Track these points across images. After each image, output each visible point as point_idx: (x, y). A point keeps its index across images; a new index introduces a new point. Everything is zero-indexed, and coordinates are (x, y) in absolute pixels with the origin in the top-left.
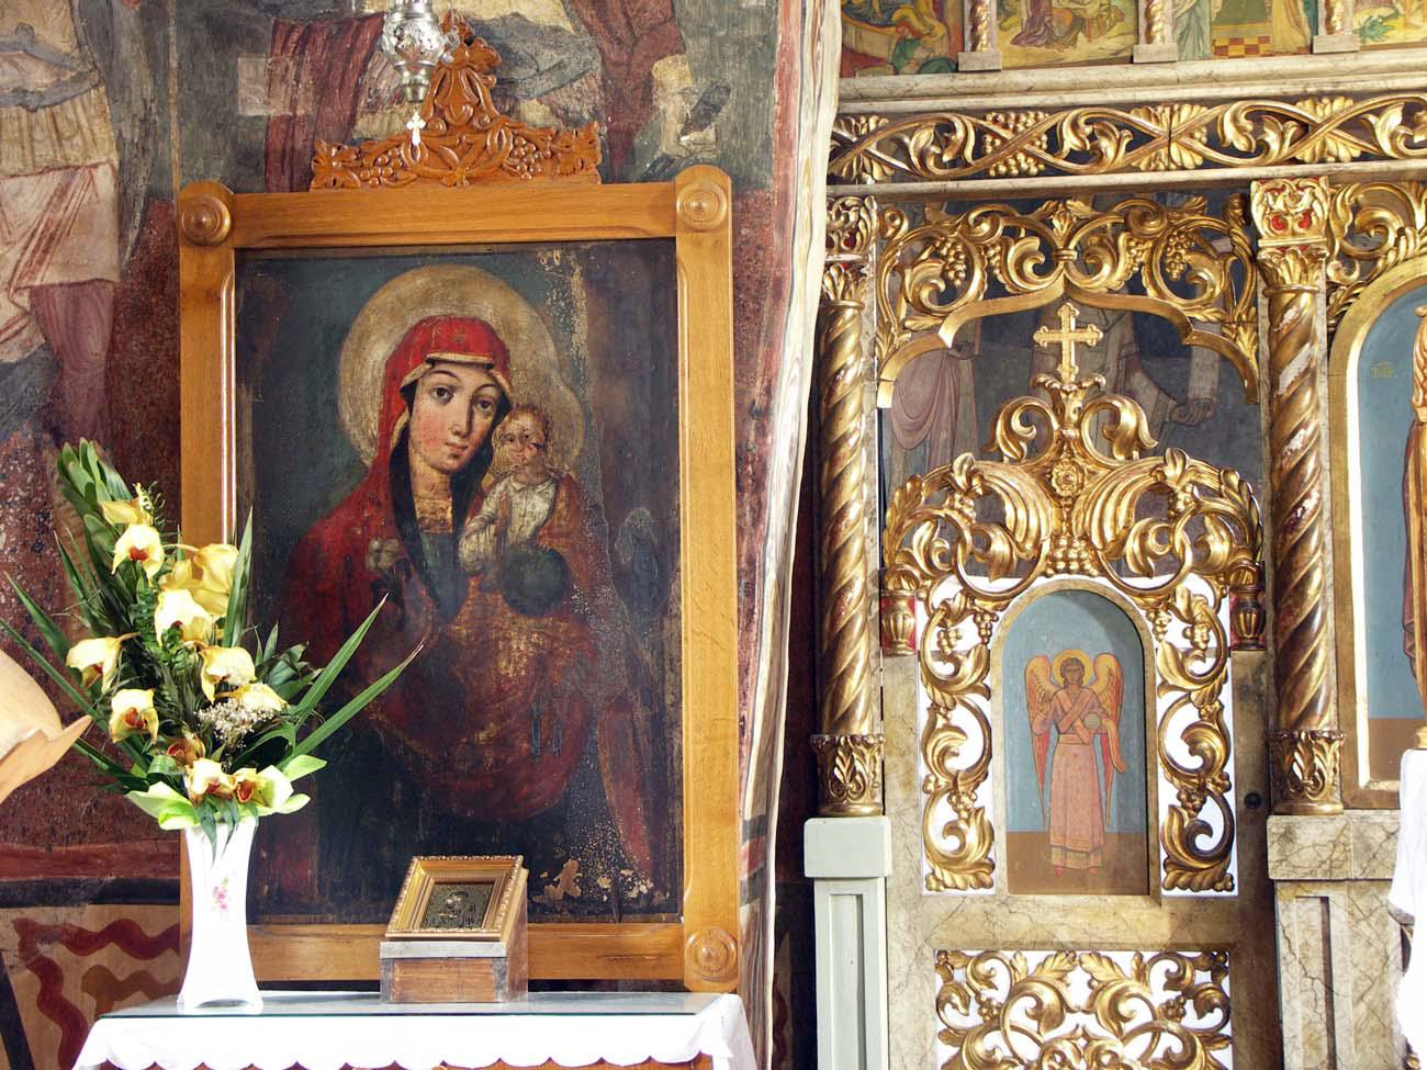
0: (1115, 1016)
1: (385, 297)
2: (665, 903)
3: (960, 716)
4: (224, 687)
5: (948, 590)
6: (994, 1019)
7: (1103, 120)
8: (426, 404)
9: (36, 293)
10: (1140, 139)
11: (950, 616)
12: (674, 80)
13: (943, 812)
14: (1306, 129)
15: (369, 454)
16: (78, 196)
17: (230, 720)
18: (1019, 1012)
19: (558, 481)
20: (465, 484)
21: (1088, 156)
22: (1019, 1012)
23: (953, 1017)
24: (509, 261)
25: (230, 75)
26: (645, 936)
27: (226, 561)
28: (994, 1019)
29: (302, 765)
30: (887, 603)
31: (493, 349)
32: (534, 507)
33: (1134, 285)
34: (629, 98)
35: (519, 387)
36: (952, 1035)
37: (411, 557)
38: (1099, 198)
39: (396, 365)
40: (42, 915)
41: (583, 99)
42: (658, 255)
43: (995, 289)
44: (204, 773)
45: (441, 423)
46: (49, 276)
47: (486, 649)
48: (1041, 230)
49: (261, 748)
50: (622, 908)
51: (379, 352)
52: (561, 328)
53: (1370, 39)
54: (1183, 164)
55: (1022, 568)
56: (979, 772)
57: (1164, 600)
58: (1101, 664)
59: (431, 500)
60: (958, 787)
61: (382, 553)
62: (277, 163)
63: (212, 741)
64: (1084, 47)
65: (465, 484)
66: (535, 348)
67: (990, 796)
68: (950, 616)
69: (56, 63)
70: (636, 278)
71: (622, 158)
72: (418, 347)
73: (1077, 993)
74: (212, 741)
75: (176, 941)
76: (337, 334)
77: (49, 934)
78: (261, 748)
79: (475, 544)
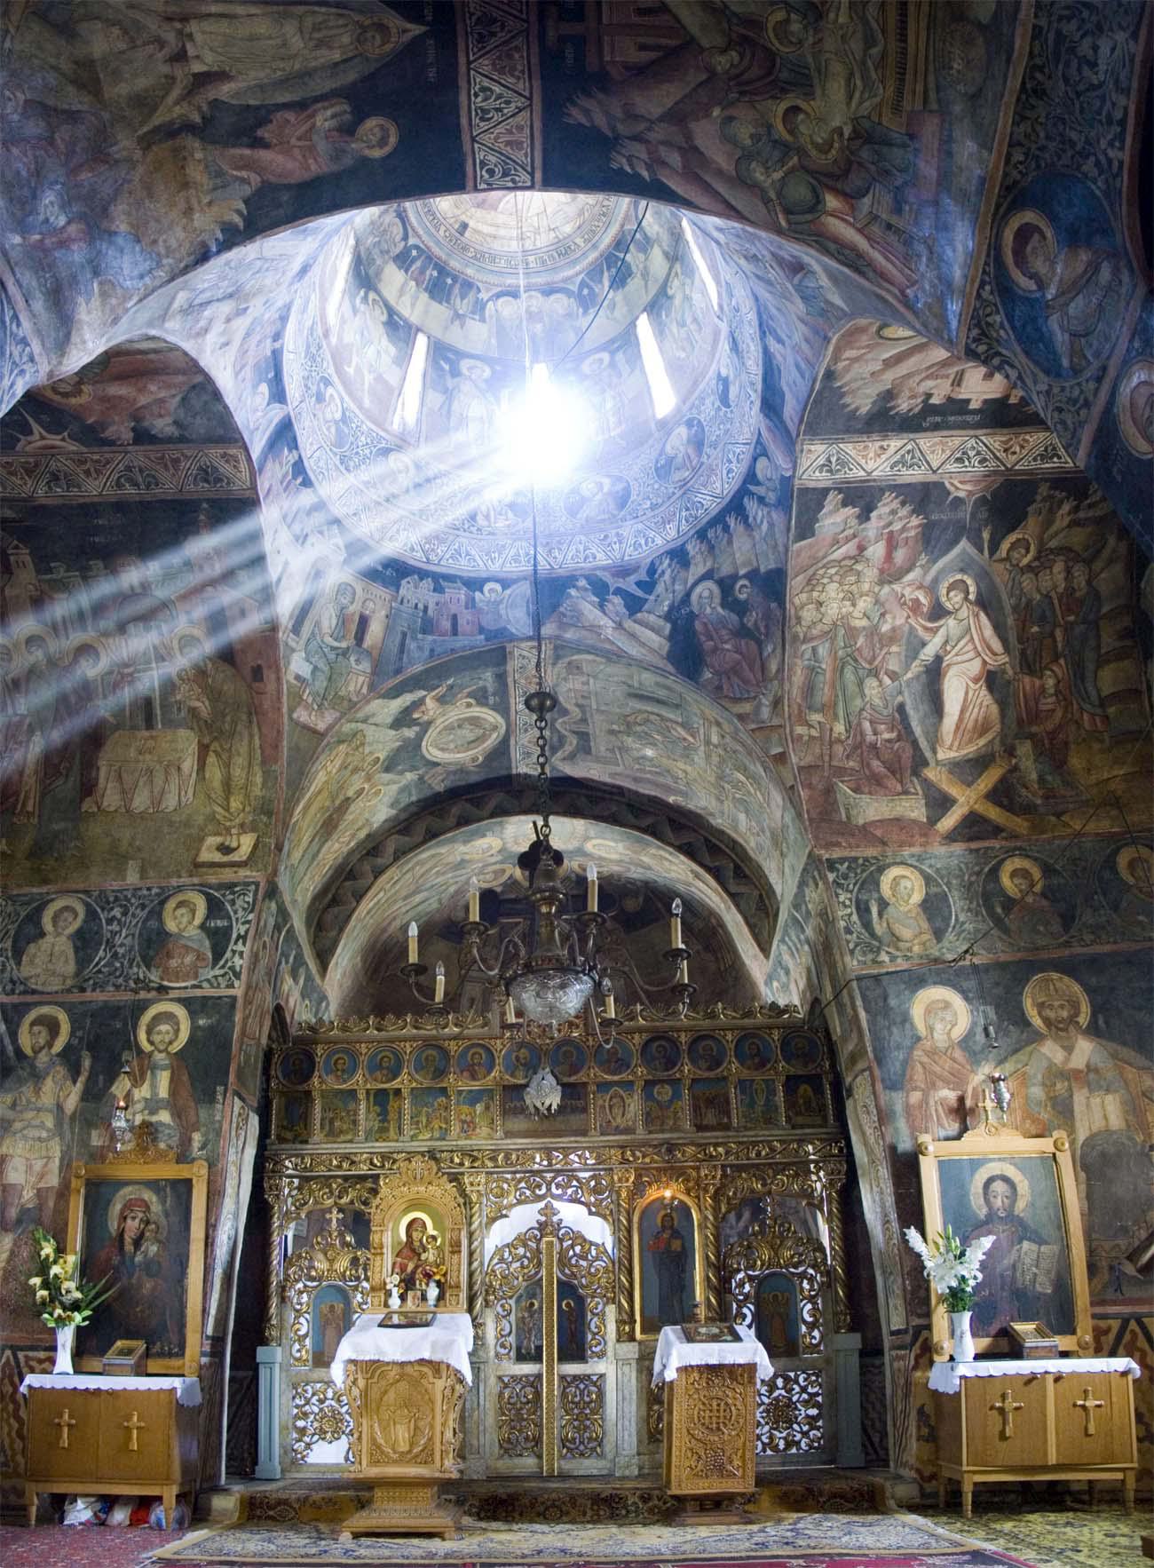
0: (339, 1401)
1: (121, 1193)
2: (181, 1354)
3: (302, 1320)
4: (68, 1292)
5: (300, 1285)
6: (308, 1402)
7: (346, 1157)
8: (129, 1221)
9: (39, 1190)
10: (353, 1163)
11: (301, 1292)
12: (197, 1138)
13: (297, 1346)
14: (395, 1161)
15: (114, 1234)
16: (50, 1165)
17: (67, 1299)
18: (314, 1400)
19: (159, 1242)
20: (137, 1243)
21: (339, 1167)
22: (314, 1400)
23: (297, 1401)
24: (154, 1185)
25: (89, 1134)
26: (175, 1362)
27: (72, 1259)
28: (308, 1402)
29: (87, 1313)
30: (283, 1289)
31: (146, 1206)
32: (154, 1248)
33: (352, 1202)
34: (186, 1142)
35: (153, 1217)
36: (297, 1407)
37: (123, 1262)
38: (346, 1178)
39: (122, 1211)
40: (31, 1354)
41: (175, 1141)
42: (188, 1183)
43: (316, 1202)
44: (58, 1311)
45: (132, 1226)
46: (41, 1185)
47: (140, 1286)
48: (330, 1186)
49: (76, 1306)
50: (170, 1355)
51: (118, 1207)
52: (163, 1202)
53: (413, 1138)
54: (364, 1169)
55: (320, 1279)
56: (306, 1336)
57: (356, 1288)
58: (340, 1307)
59: (129, 1247)
60: (301, 1339)
61: (116, 1260)
62: (98, 1156)
63: (62, 1303)
64: (342, 1138)
65: (137, 1243)
66: (156, 1208)
67: (308, 1341)
68: (301, 1292)
69: (48, 1130)
70: (182, 1189)
71: (183, 1158)
72: (129, 1205)
73: (330, 1394)
74: (62, 1303)
75: (53, 1362)
76: (109, 1202)
77: (33, 1359)
78: (76, 1306)
79: (139, 1258)
